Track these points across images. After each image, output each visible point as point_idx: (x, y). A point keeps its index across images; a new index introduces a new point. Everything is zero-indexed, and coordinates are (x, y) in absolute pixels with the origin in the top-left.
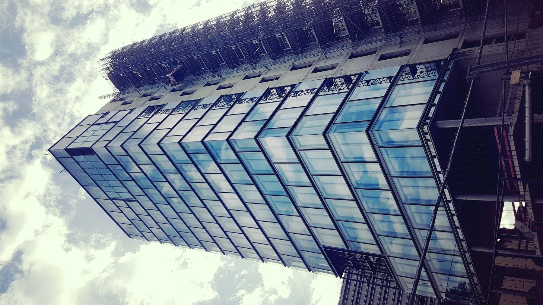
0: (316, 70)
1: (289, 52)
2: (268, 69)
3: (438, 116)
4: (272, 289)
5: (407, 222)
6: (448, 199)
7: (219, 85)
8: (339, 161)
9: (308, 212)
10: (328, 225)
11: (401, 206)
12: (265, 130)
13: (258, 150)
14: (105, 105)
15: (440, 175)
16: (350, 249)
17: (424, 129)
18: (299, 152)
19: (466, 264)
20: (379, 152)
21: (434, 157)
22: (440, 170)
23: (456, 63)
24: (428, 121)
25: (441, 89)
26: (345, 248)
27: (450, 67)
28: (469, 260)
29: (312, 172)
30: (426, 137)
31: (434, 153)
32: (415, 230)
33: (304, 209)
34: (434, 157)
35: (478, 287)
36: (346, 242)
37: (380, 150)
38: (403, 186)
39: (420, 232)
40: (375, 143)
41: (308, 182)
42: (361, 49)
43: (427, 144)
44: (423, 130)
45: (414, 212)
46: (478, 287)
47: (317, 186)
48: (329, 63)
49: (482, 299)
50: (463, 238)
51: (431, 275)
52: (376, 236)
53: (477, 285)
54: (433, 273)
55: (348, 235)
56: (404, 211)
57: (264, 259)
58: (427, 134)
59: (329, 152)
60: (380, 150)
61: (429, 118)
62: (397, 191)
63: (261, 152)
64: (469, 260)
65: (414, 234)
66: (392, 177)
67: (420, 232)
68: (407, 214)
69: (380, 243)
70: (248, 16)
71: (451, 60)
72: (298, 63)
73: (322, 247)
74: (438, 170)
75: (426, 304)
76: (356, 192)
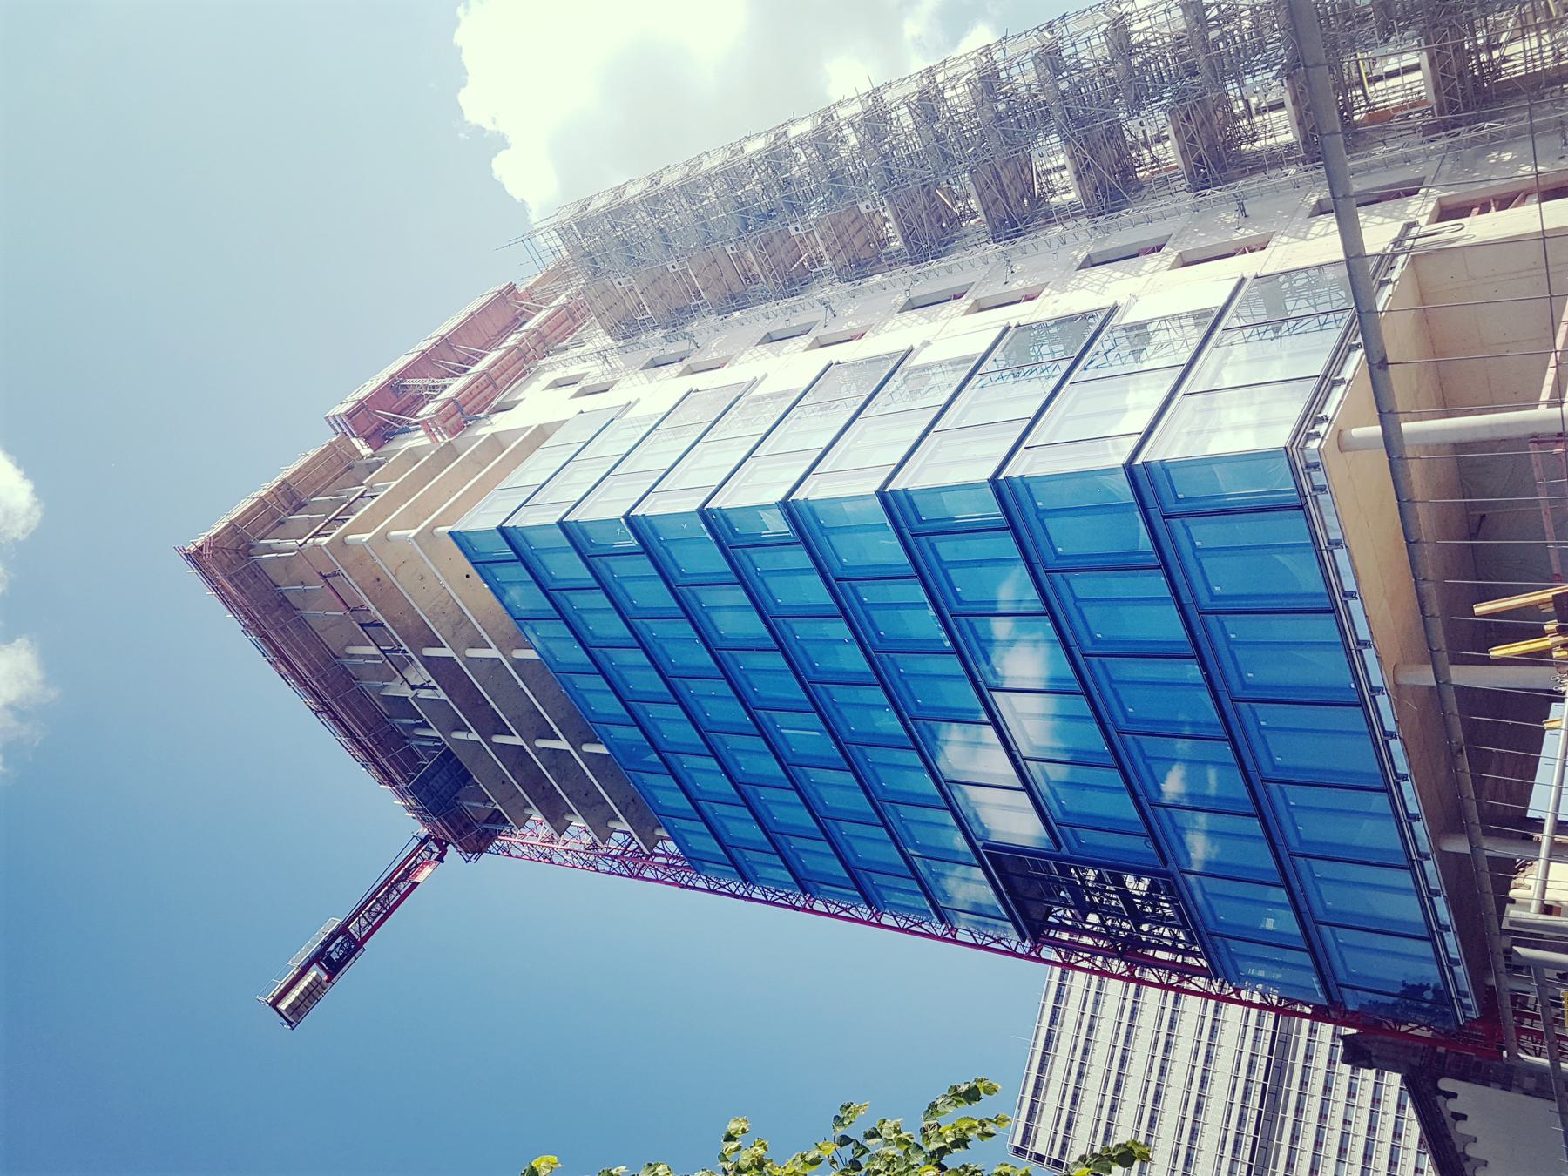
0: (979, 307)
1: (893, 261)
2: (833, 311)
4: (1030, 249)
6: (1374, 684)
7: (685, 363)
10: (1059, 517)
11: (1228, 707)
14: (499, 155)
15: (1352, 603)
16: (1065, 850)
27: (1395, 275)
31: (1336, 530)
35: (1459, 970)
38: (1235, 643)
39: (1281, 790)
42: (1116, 241)
46: (1459, 970)
48: (1018, 285)
49: (1469, 1008)
50: (1417, 811)
53: (1457, 963)
55: (1061, 806)
57: (811, 886)
65: (1264, 801)
67: (1281, 790)
70: (776, 157)
71: (1395, 255)
72: (922, 290)
73: (979, 844)
75: (1274, 1174)
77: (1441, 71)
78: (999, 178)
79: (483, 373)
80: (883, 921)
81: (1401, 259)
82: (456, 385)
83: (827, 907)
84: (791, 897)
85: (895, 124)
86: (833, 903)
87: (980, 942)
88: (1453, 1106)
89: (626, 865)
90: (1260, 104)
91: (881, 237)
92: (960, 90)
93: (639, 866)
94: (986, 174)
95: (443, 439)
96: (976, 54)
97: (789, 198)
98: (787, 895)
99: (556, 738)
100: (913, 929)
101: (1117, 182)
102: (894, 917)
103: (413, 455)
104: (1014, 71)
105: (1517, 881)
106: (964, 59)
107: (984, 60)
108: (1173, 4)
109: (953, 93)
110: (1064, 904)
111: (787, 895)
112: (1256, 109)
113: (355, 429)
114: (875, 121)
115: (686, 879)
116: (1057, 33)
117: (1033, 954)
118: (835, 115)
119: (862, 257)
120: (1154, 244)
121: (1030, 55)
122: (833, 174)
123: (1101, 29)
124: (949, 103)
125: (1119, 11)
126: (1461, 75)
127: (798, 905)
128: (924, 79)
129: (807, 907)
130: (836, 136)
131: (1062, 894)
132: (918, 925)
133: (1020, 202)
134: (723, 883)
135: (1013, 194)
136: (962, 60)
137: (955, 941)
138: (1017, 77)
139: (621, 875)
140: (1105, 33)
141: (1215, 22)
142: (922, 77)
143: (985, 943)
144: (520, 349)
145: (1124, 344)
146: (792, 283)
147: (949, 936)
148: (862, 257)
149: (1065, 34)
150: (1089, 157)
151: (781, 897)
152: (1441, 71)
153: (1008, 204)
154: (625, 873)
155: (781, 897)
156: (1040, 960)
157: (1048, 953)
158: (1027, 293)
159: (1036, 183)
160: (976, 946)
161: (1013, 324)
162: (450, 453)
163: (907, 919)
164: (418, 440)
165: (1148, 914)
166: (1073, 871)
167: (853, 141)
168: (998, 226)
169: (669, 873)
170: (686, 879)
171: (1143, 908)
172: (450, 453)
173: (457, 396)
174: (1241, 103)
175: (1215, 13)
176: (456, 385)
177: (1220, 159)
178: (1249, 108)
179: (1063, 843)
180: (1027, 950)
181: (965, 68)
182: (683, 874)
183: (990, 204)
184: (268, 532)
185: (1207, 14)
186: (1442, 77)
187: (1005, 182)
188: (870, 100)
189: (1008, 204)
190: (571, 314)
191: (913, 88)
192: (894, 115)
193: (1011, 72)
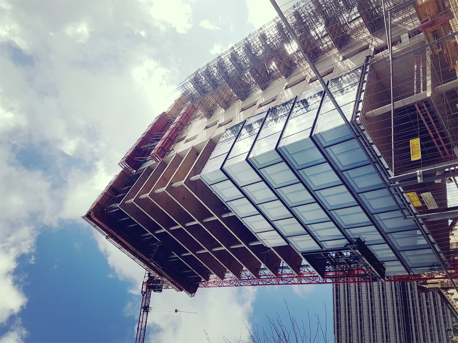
3: (365, 109)
5: (392, 247)
8: (311, 190)
9: (295, 240)
12: (228, 160)
13: (226, 179)
16: (324, 249)
17: (357, 121)
18: (259, 171)
19: (425, 235)
20: (325, 153)
21: (372, 144)
22: (364, 128)
23: (372, 67)
24: (359, 114)
25: (364, 88)
26: (319, 248)
27: (367, 70)
28: (427, 231)
29: (306, 223)
30: (361, 128)
32: (359, 195)
33: (276, 222)
34: (372, 144)
36: (290, 209)
37: (325, 150)
40: (320, 145)
41: (289, 214)
43: (387, 172)
44: (356, 123)
45: (337, 154)
47: (253, 163)
51: (398, 254)
52: (343, 230)
54: (411, 269)
56: (360, 201)
58: (364, 130)
59: (301, 185)
60: (325, 150)
61: (359, 112)
62: (349, 183)
63: (229, 180)
64: (427, 231)
66: (357, 194)
68: (380, 226)
69: (333, 217)
71: (366, 65)
74: (386, 168)
76: (299, 173)
77: (366, 16)
78: (258, 72)
79: (167, 137)
80: (302, 282)
81: (368, 67)
82: (159, 144)
83: (263, 283)
84: (252, 282)
85: (227, 64)
86: (264, 281)
87: (309, 282)
88: (453, 297)
89: (203, 284)
90: (322, 35)
91: (231, 94)
92: (242, 51)
93: (206, 283)
94: (254, 71)
95: (160, 160)
96: (258, 31)
97: (203, 90)
98: (251, 282)
99: (188, 252)
100: (289, 283)
101: (289, 65)
102: (306, 280)
103: (150, 169)
104: (255, 42)
105: (454, 228)
106: (241, 42)
107: (246, 41)
108: (292, 15)
109: (240, 52)
110: (328, 265)
111: (251, 282)
112: (321, 37)
113: (164, 145)
114: (221, 65)
115: (221, 284)
116: (263, 30)
117: (325, 282)
118: (210, 65)
119: (227, 101)
120: (303, 79)
121: (258, 37)
122: (213, 80)
123: (275, 26)
124: (239, 55)
125: (278, 20)
126: (371, 16)
127: (254, 284)
128: (231, 51)
129: (257, 284)
130: (212, 71)
131: (327, 262)
132: (290, 281)
133: (265, 77)
134: (231, 283)
135: (263, 75)
136: (240, 43)
137: (302, 284)
138: (256, 44)
139: (202, 287)
140: (276, 27)
141: (304, 17)
142: (230, 50)
143: (310, 282)
144: (176, 128)
145: (302, 106)
146: (210, 112)
147: (300, 283)
148: (227, 101)
149: (266, 29)
150: (280, 60)
151: (249, 283)
152: (366, 16)
153: (262, 78)
154: (203, 286)
155: (249, 283)
156: (327, 283)
157: (329, 280)
158: (328, 72)
159: (268, 71)
160: (308, 283)
161: (271, 108)
162: (164, 165)
163: (287, 281)
164: (151, 163)
165: (352, 262)
166: (329, 255)
167: (216, 71)
168: (260, 84)
169: (215, 284)
170: (221, 284)
171: (350, 260)
172: (164, 165)
173: (162, 145)
174: (317, 37)
175: (303, 15)
176: (159, 144)
177: (315, 52)
178: (319, 37)
179: (323, 247)
180: (322, 281)
181: (242, 45)
182: (219, 283)
183: (257, 79)
184: (110, 203)
185: (301, 16)
186: (367, 17)
187: (260, 72)
188: (218, 59)
189: (262, 78)
190: (187, 115)
191: (229, 53)
192: (226, 62)
193: (254, 43)
